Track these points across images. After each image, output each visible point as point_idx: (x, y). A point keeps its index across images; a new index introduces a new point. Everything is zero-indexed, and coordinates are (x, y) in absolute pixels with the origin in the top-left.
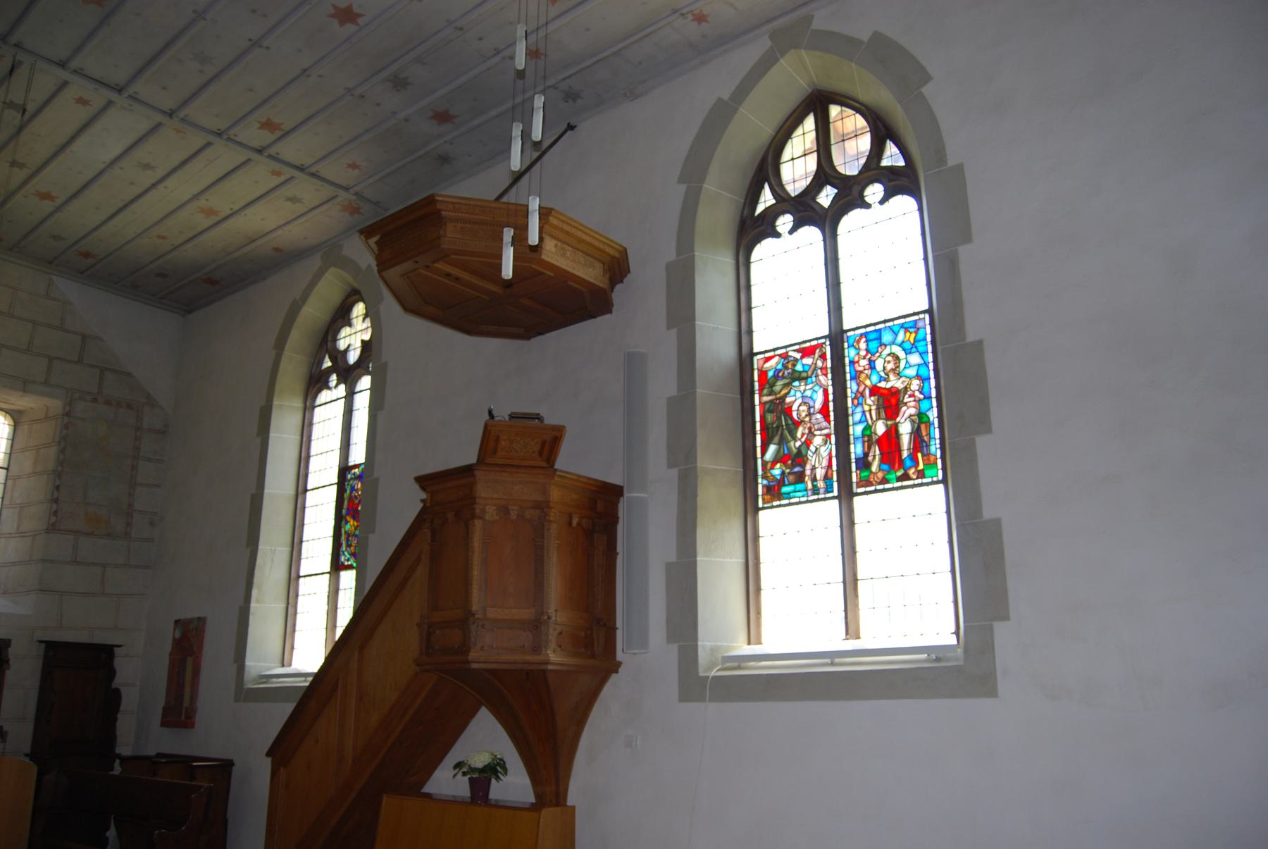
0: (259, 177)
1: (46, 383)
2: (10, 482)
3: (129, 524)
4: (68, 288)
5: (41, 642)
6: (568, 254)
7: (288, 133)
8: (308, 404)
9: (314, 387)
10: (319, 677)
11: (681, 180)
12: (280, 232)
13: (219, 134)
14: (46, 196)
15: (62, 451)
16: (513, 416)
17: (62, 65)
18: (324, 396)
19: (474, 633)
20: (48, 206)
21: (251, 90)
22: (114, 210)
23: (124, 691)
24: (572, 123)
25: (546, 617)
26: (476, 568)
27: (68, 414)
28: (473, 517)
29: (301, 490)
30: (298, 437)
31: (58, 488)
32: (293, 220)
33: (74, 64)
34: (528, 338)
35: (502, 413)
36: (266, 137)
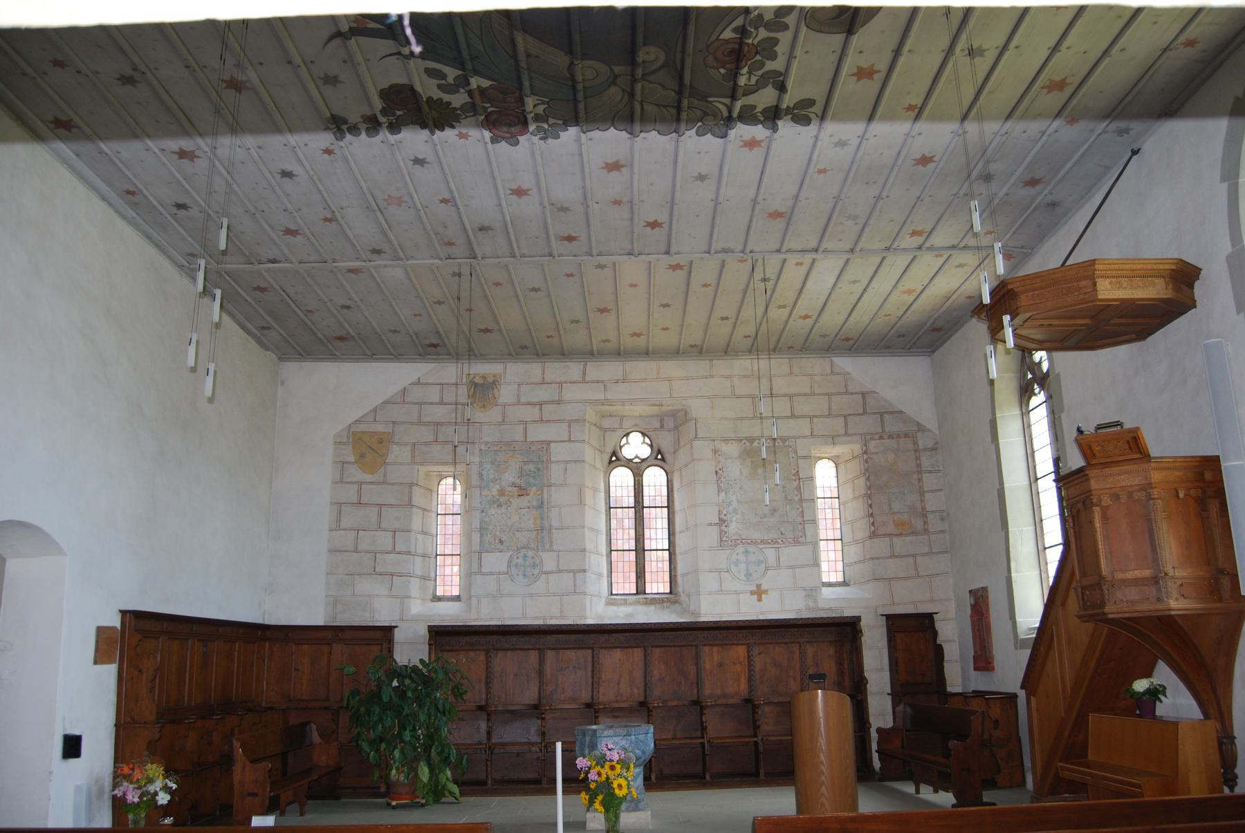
0: (928, 264)
1: (846, 434)
2: (842, 507)
3: (925, 523)
4: (844, 363)
5: (882, 615)
6: (1125, 284)
7: (931, 232)
8: (1024, 411)
9: (1025, 396)
10: (1041, 630)
11: (1223, 180)
12: (963, 288)
13: (888, 249)
14: (806, 317)
15: (868, 479)
16: (1099, 427)
17: (779, 251)
18: (1034, 401)
19: (1106, 592)
20: (809, 322)
21: (892, 221)
22: (849, 311)
23: (946, 647)
24: (1136, 148)
25: (1163, 574)
26: (1100, 543)
27: (865, 452)
28: (1093, 505)
29: (1034, 479)
30: (1022, 439)
31: (871, 506)
32: (970, 276)
33: (784, 249)
34: (1144, 338)
35: (1089, 428)
36: (918, 240)
